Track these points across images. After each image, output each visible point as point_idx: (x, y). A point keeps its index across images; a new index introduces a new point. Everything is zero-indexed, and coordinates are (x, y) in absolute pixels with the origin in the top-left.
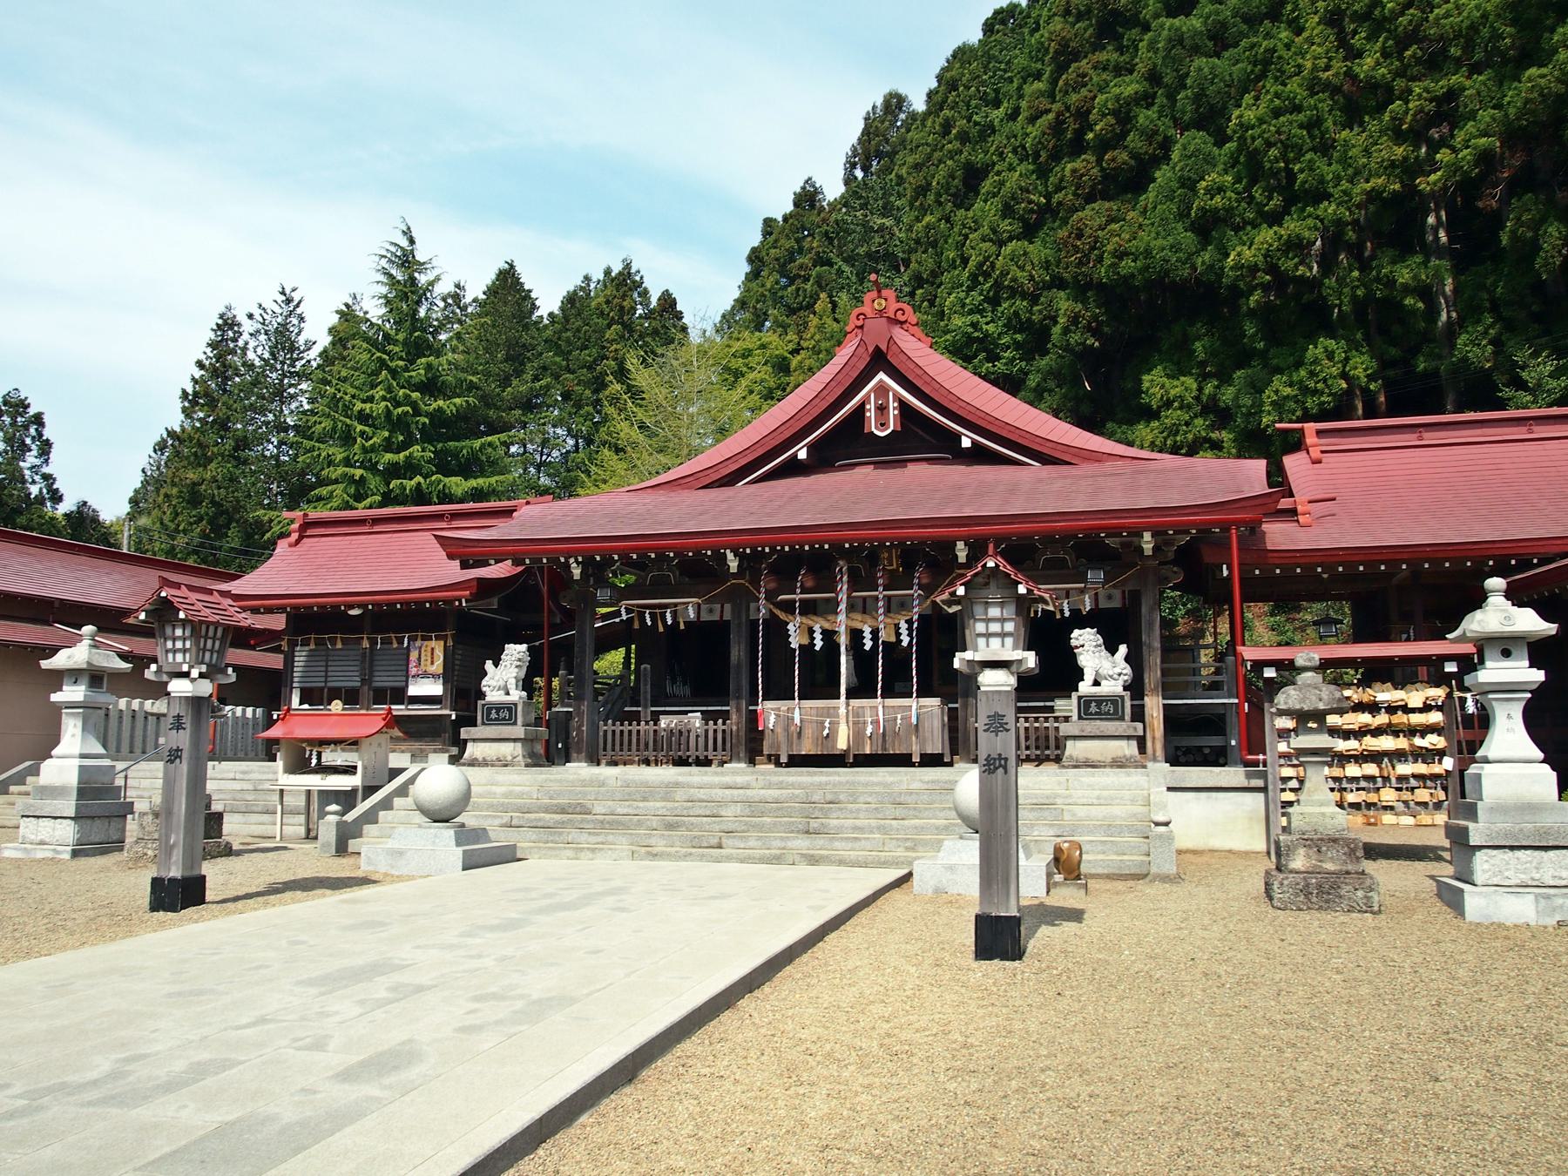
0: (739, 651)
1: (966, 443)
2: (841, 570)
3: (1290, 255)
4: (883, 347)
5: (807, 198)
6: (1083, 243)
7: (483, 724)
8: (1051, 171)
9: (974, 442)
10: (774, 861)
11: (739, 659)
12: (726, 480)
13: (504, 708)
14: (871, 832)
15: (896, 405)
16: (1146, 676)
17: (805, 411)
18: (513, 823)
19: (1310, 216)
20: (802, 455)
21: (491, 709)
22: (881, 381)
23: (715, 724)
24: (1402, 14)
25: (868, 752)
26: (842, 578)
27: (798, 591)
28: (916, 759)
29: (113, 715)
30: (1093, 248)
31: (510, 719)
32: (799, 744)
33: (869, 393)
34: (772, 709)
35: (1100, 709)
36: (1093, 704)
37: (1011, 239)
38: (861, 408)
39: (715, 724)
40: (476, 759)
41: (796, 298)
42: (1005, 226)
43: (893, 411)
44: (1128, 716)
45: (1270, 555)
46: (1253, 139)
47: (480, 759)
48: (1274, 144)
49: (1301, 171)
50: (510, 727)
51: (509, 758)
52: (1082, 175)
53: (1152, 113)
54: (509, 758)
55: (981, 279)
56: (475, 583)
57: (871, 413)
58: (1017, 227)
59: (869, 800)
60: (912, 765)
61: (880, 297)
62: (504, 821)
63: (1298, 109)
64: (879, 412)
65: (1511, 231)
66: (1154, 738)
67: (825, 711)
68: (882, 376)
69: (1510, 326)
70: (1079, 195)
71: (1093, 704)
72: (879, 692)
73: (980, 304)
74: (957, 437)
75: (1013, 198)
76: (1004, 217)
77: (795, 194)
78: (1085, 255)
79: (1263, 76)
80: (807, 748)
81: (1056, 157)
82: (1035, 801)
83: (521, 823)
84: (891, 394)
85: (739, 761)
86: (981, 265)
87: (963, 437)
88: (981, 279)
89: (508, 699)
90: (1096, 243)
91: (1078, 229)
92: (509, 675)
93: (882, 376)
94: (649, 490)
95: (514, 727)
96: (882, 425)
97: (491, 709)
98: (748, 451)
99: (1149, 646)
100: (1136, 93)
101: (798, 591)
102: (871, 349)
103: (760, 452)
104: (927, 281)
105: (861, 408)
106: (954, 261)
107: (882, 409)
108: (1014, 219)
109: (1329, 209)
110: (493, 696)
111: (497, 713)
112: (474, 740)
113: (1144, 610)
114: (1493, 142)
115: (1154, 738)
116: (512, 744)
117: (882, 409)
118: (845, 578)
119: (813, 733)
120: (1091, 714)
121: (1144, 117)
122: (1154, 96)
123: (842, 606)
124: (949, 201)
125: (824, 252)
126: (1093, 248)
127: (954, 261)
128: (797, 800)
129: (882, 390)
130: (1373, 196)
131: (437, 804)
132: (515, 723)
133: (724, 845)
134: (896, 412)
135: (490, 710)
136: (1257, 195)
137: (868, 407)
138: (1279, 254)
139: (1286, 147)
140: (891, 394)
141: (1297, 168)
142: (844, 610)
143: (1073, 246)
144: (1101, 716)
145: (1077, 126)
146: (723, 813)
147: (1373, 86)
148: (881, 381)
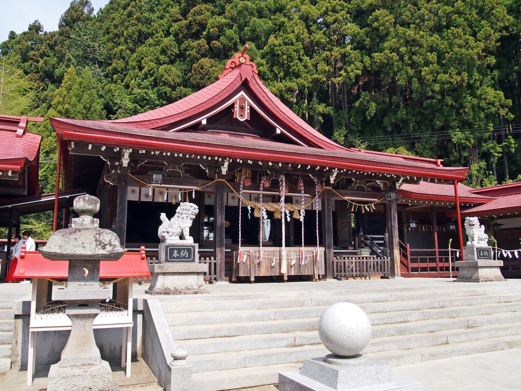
0: (222, 218)
1: (278, 131)
2: (281, 180)
3: (289, 93)
4: (249, 79)
5: (36, 28)
6: (203, 71)
7: (167, 261)
8: (183, 42)
9: (281, 132)
10: (494, 349)
11: (221, 223)
12: (165, 127)
13: (184, 249)
14: (495, 323)
15: (248, 108)
16: (394, 240)
17: (211, 101)
18: (297, 343)
19: (294, 82)
20: (204, 122)
21: (174, 249)
22: (242, 95)
23: (210, 259)
24: (333, 24)
25: (293, 274)
26: (282, 183)
27: (261, 188)
28: (253, 279)
29: (330, 239)
30: (207, 74)
31: (189, 257)
32: (259, 271)
33: (237, 99)
34: (244, 251)
35: (180, 254)
36: (176, 251)
37: (164, 63)
38: (232, 106)
39: (210, 259)
40: (167, 289)
41: (30, 68)
42: (162, 58)
43: (247, 111)
44: (492, 258)
45: (413, 194)
46: (277, 50)
47: (172, 289)
48: (285, 54)
49: (293, 66)
50: (189, 264)
51: (196, 287)
52: (201, 47)
53: (232, 31)
54: (196, 287)
55: (149, 76)
56: (24, 161)
57: (237, 109)
58: (167, 60)
59: (458, 304)
60: (250, 282)
61: (243, 56)
62: (289, 342)
63: (292, 44)
64: (241, 109)
65: (361, 102)
66: (397, 266)
67: (272, 253)
68: (242, 93)
69: (351, 131)
70: (199, 53)
71: (176, 251)
72: (303, 244)
73: (148, 86)
74: (275, 128)
75: (167, 48)
76: (161, 54)
77: (30, 25)
78: (203, 76)
79: (279, 30)
80: (263, 272)
81: (186, 37)
82: (518, 299)
83: (303, 342)
84: (246, 102)
85: (222, 280)
86: (150, 71)
87: (277, 129)
88: (149, 76)
89: (182, 242)
90: (208, 72)
91: (202, 65)
92: (185, 225)
93: (242, 93)
94: (124, 124)
95: (193, 264)
96: (242, 116)
97: (174, 249)
98: (181, 114)
99: (394, 227)
100: (226, 22)
101: (261, 188)
102: (243, 79)
103: (187, 116)
104: (119, 72)
105: (232, 106)
106: (135, 67)
107: (242, 108)
108: (166, 56)
109: (301, 80)
110: (172, 240)
111: (179, 252)
112: (164, 274)
113: (392, 212)
114: (359, 72)
115: (397, 266)
116: (196, 277)
117: (242, 108)
118: (284, 184)
119: (266, 265)
120: (174, 258)
121: (229, 32)
122: (233, 26)
123: (283, 199)
124: (131, 43)
125: (47, 52)
126: (207, 74)
127: (135, 67)
128: (428, 307)
129: (242, 99)
130: (316, 81)
131: (330, 333)
132: (193, 261)
133: (449, 342)
134: (248, 111)
135: (172, 251)
136: (275, 70)
137: (236, 106)
138: (284, 92)
139: (288, 56)
140: (246, 102)
141: (292, 64)
142: (284, 200)
143: (199, 71)
144: (180, 259)
145: (198, 28)
146: (410, 319)
147: (318, 44)
148: (242, 95)
